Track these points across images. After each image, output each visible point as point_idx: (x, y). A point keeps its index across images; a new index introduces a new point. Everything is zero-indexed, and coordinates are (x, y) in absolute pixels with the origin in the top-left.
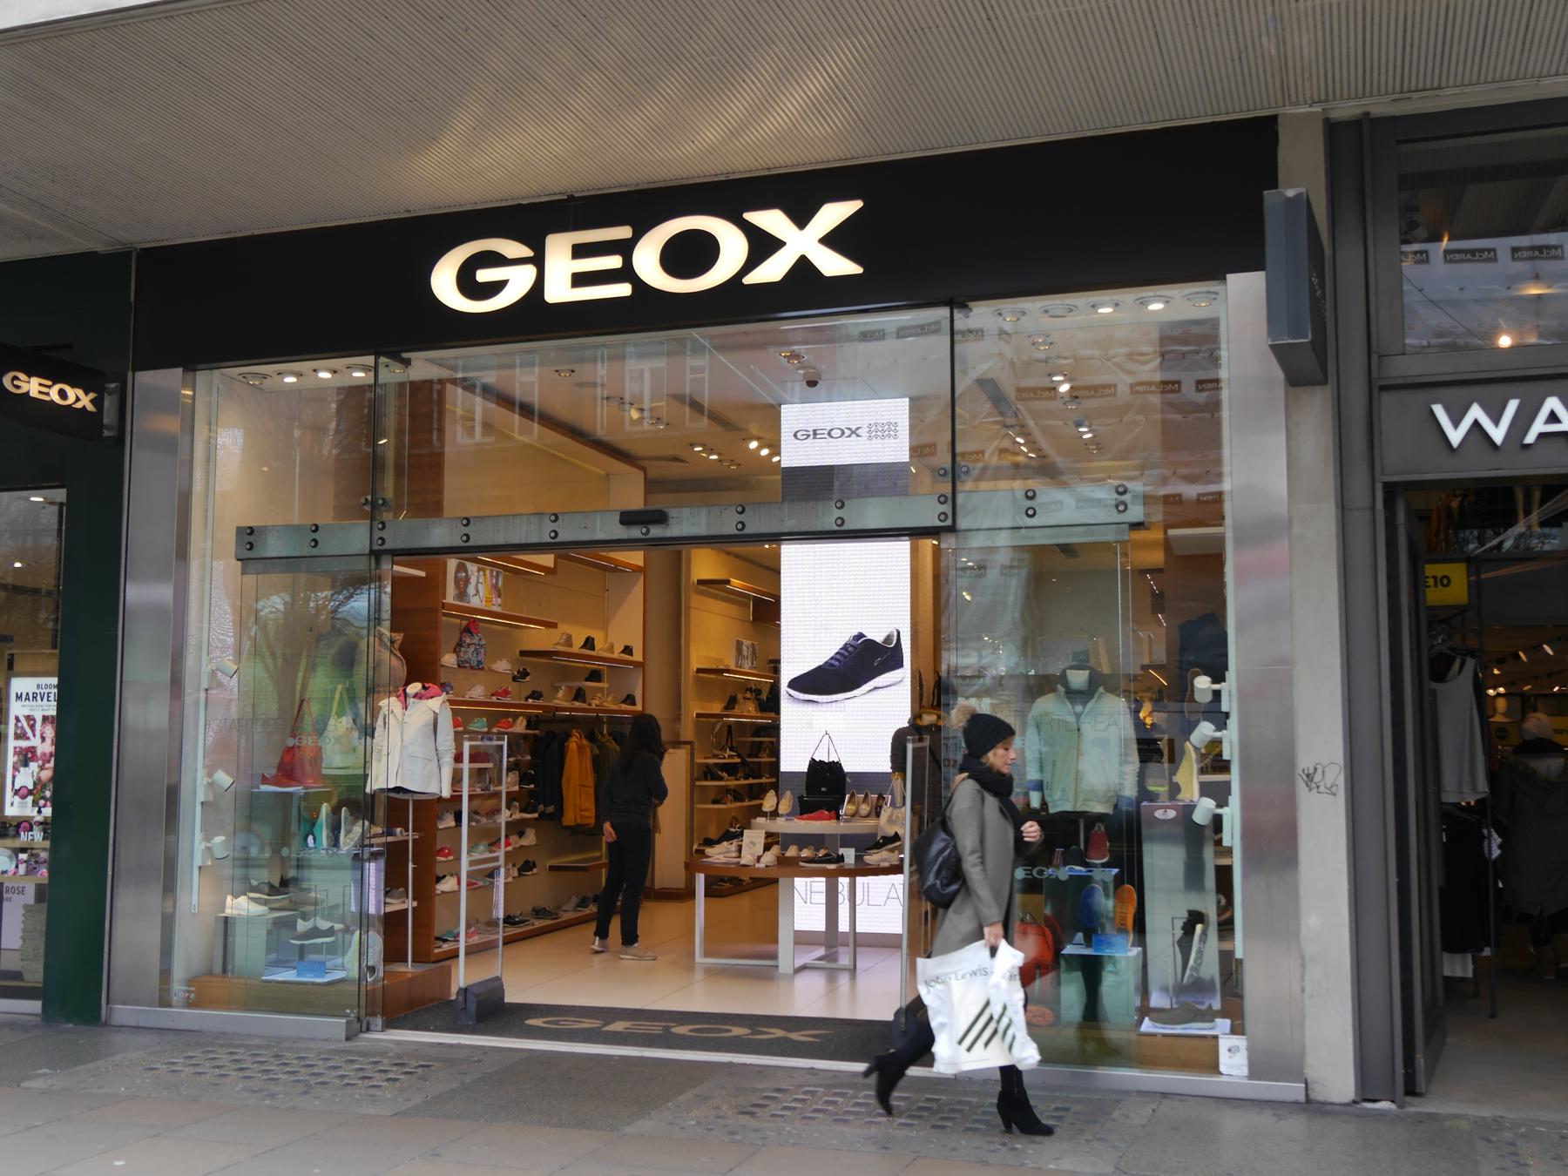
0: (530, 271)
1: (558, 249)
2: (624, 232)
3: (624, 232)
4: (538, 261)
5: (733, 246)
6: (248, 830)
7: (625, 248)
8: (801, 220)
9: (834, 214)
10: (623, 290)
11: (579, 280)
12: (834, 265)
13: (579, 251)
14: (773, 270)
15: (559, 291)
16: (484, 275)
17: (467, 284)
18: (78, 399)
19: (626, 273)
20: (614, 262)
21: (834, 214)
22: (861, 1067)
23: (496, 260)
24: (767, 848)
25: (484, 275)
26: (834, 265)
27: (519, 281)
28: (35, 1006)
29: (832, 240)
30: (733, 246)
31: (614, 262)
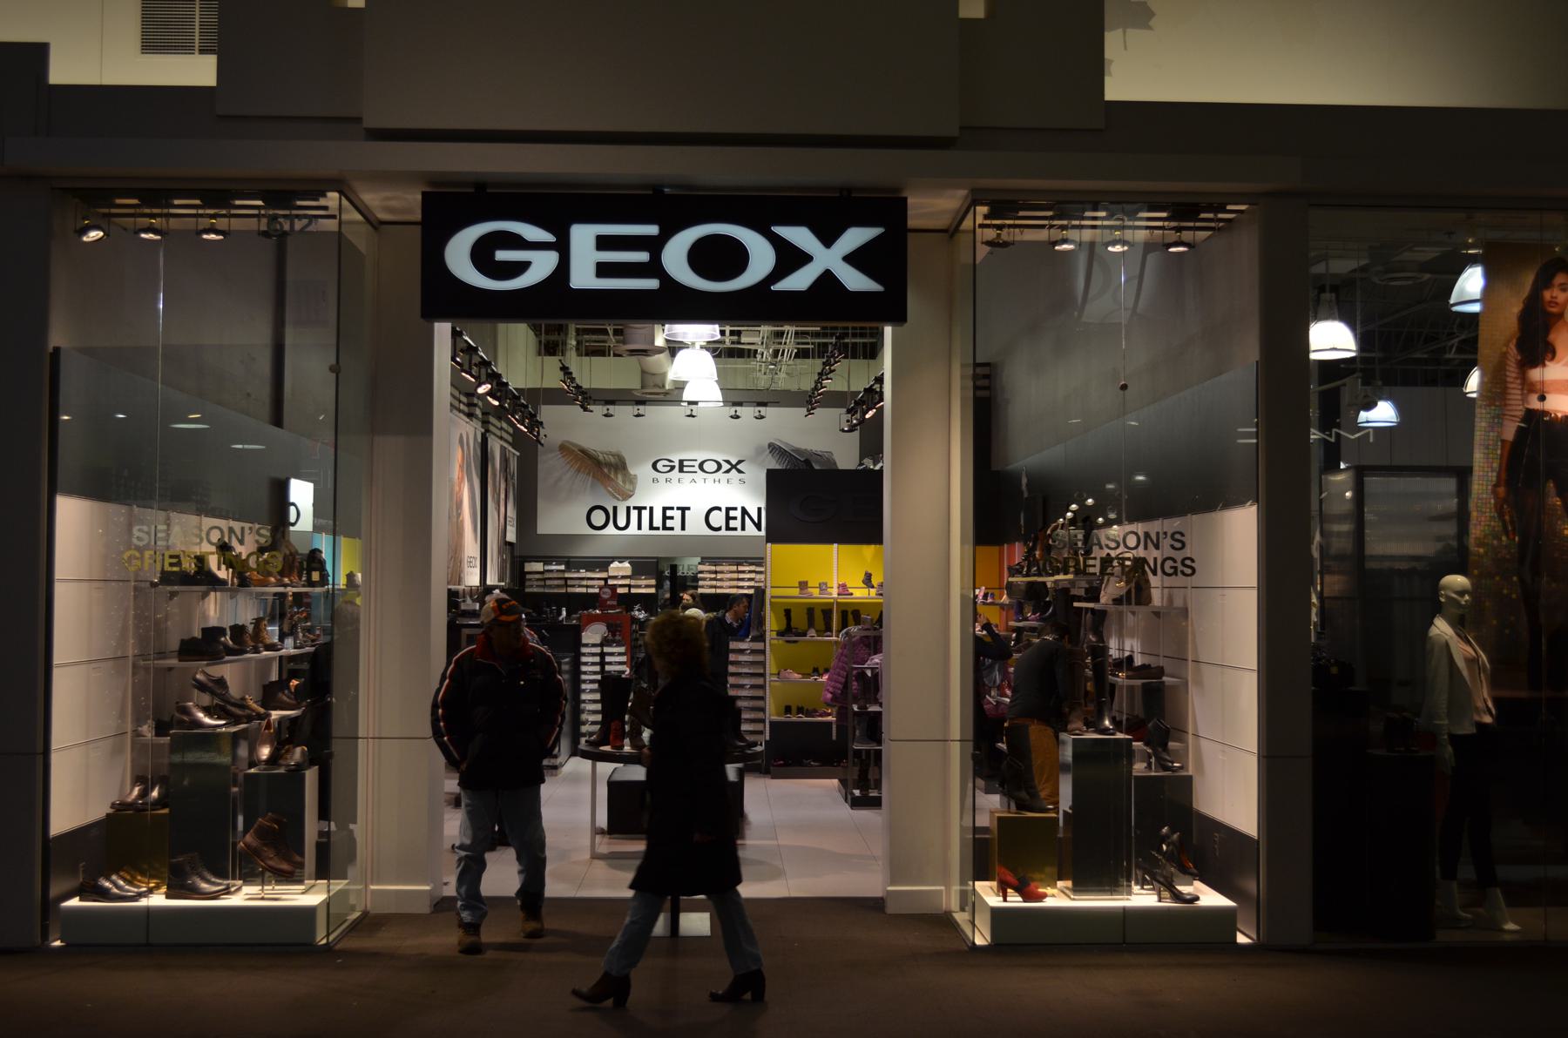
1: (583, 236)
2: (652, 230)
3: (652, 230)
4: (562, 247)
7: (654, 246)
8: (828, 240)
9: (855, 237)
10: (652, 284)
12: (855, 281)
13: (603, 243)
14: (799, 281)
15: (583, 277)
16: (502, 255)
17: (482, 255)
18: (790, 258)
19: (654, 268)
20: (642, 257)
21: (855, 237)
23: (518, 242)
25: (502, 255)
26: (855, 281)
27: (542, 265)
31: (642, 257)
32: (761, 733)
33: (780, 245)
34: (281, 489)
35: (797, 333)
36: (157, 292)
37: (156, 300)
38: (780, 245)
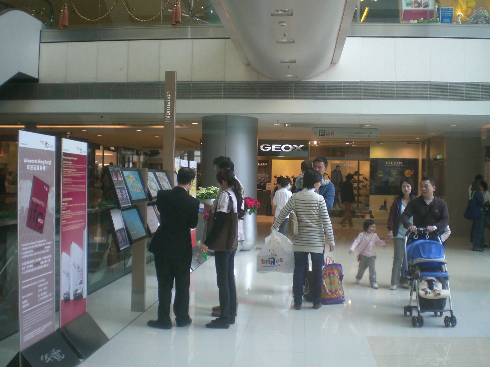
0: (271, 148)
1: (391, 162)
2: (280, 145)
3: (280, 145)
5: (264, 164)
6: (69, 293)
7: (281, 147)
9: (402, 162)
10: (280, 150)
11: (275, 149)
12: (402, 164)
13: (276, 147)
14: (400, 164)
15: (273, 150)
16: (266, 148)
17: (387, 163)
19: (281, 149)
20: (279, 148)
21: (402, 162)
22: (122, 206)
24: (200, 189)
25: (266, 148)
26: (402, 164)
28: (407, 270)
30: (264, 164)
31: (279, 148)
32: (276, 147)
34: (163, 125)
35: (191, 27)
36: (172, 287)
37: (289, 77)
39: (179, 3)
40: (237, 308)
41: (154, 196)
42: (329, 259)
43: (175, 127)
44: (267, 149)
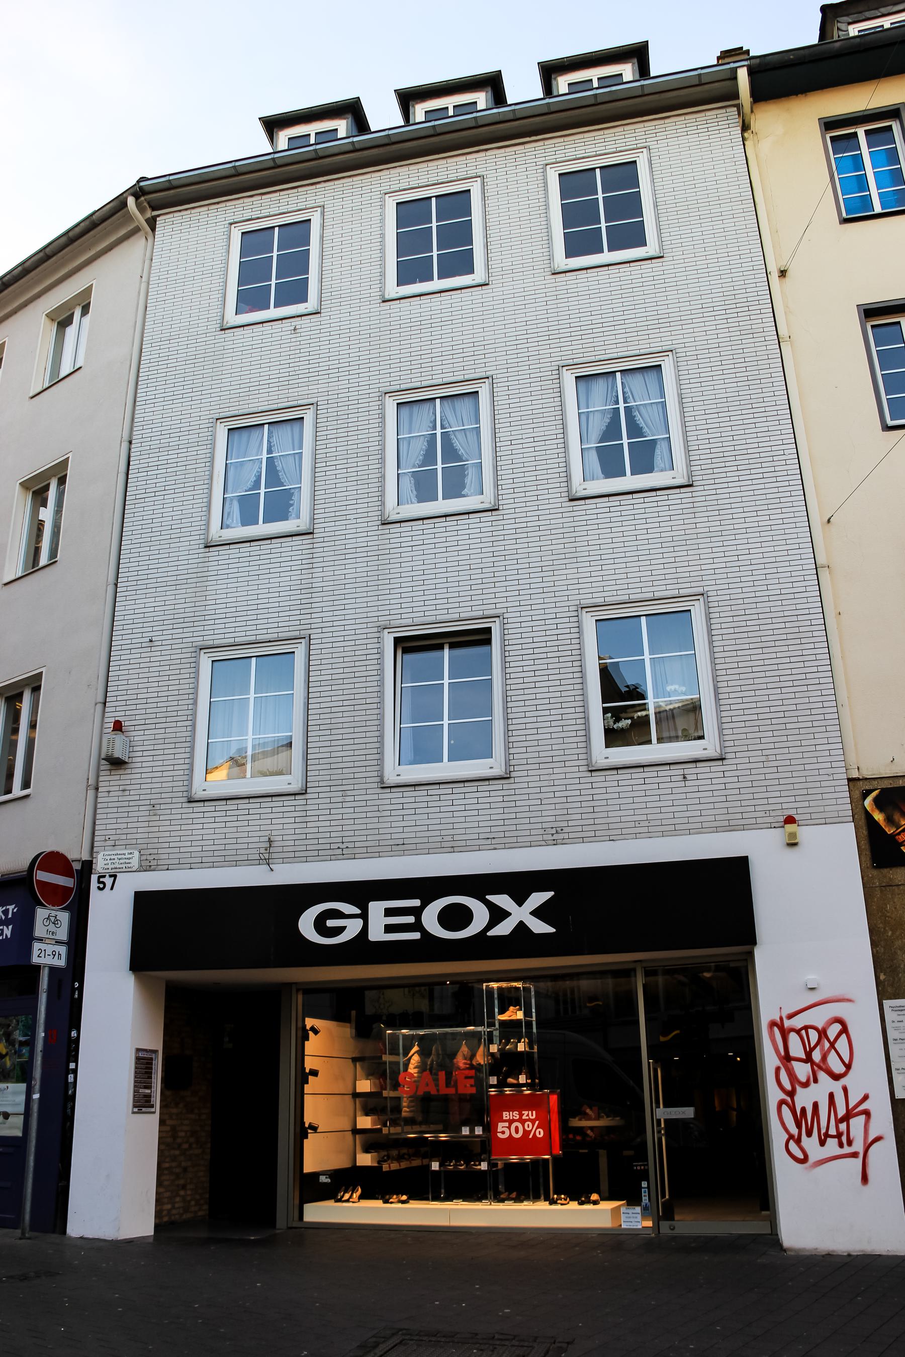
0: (359, 922)
2: (416, 903)
3: (416, 903)
4: (364, 916)
5: (481, 915)
7: (417, 912)
8: (520, 901)
9: (538, 899)
10: (416, 936)
11: (389, 929)
12: (539, 927)
13: (389, 912)
14: (504, 929)
15: (377, 934)
16: (330, 923)
17: (320, 925)
19: (417, 926)
20: (411, 919)
21: (538, 899)
25: (330, 923)
26: (539, 927)
27: (353, 928)
29: (536, 913)
30: (481, 915)
31: (411, 919)
32: (389, 912)
33: (491, 906)
38: (491, 906)
39: (385, 1125)
40: (804, 1250)
41: (91, 1232)
42: (787, 1136)
43: (527, 1013)
44: (342, 929)
